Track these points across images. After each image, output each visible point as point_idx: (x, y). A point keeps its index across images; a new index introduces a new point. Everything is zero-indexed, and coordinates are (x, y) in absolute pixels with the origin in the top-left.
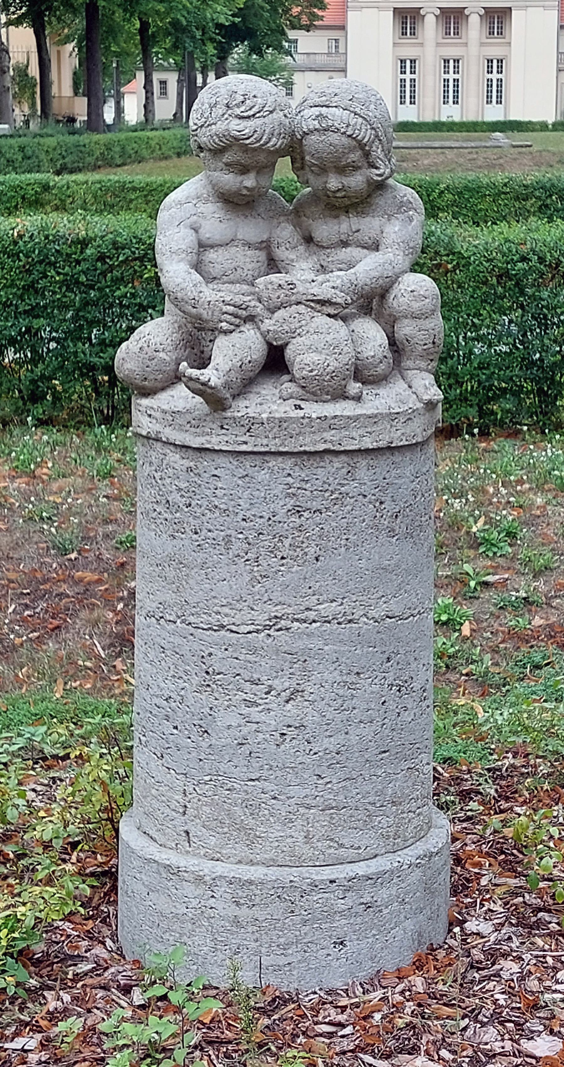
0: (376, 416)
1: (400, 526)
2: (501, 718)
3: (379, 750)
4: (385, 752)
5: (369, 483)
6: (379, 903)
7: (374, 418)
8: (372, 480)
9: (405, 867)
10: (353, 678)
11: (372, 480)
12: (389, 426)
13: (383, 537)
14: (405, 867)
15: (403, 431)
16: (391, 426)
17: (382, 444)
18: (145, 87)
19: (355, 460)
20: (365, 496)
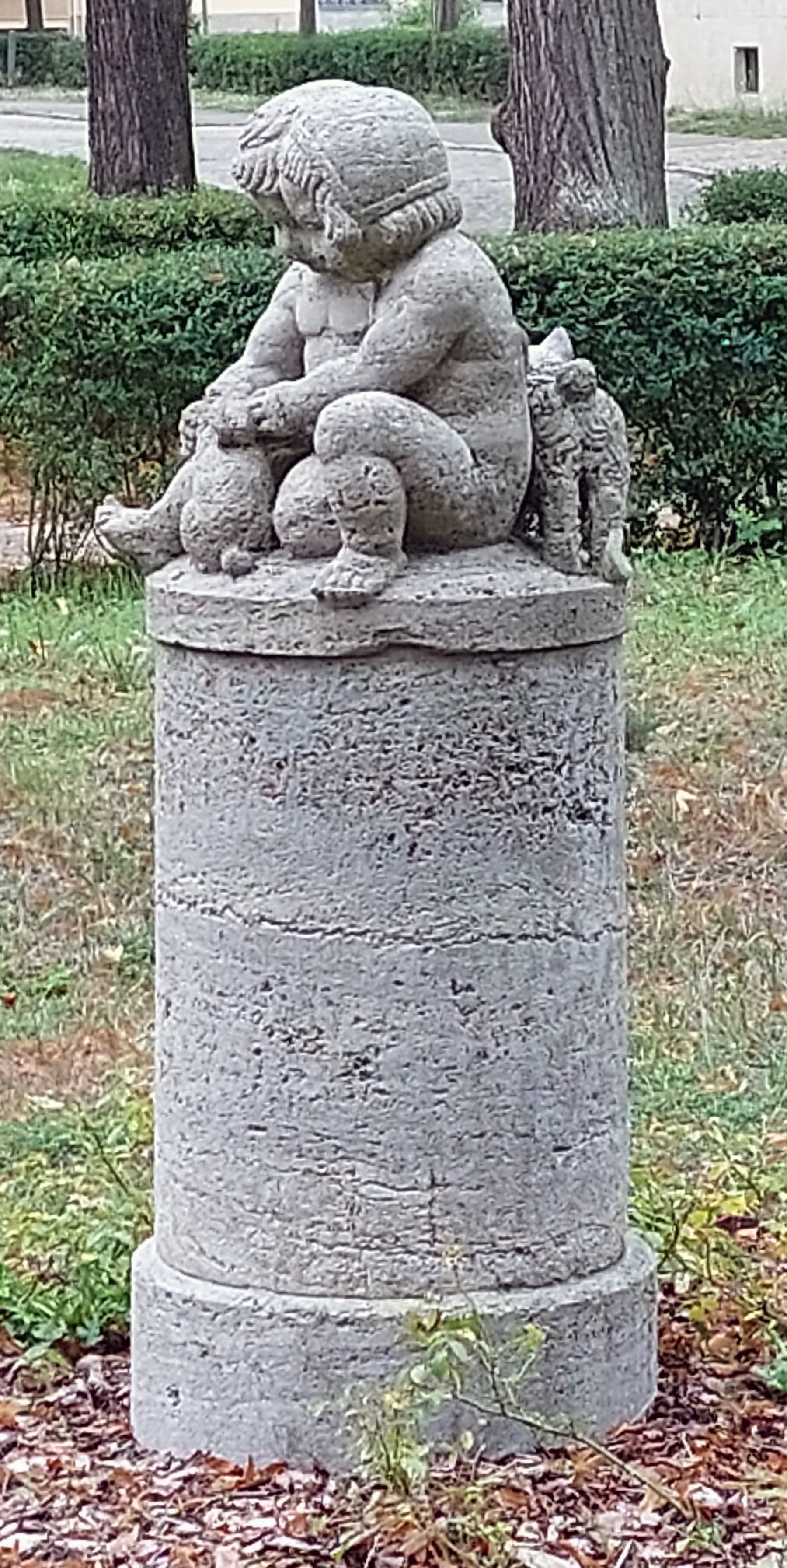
0: (225, 601)
1: (289, 782)
2: (774, 1230)
3: (248, 1122)
4: (257, 1128)
5: (233, 705)
6: (217, 1352)
7: (253, 608)
8: (237, 701)
9: (263, 1313)
10: (213, 1000)
11: (237, 701)
12: (245, 622)
13: (253, 793)
14: (263, 1313)
15: (272, 632)
16: (250, 621)
17: (237, 647)
18: (668, 63)
19: (215, 665)
20: (226, 724)
